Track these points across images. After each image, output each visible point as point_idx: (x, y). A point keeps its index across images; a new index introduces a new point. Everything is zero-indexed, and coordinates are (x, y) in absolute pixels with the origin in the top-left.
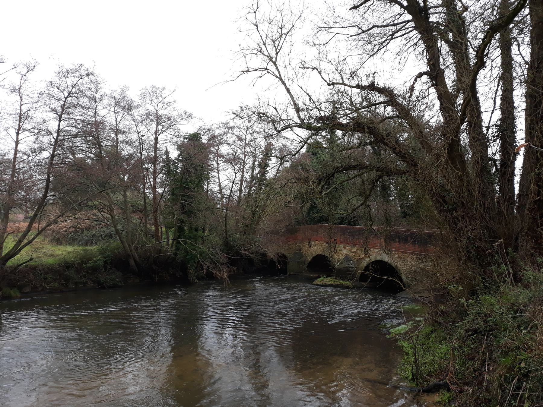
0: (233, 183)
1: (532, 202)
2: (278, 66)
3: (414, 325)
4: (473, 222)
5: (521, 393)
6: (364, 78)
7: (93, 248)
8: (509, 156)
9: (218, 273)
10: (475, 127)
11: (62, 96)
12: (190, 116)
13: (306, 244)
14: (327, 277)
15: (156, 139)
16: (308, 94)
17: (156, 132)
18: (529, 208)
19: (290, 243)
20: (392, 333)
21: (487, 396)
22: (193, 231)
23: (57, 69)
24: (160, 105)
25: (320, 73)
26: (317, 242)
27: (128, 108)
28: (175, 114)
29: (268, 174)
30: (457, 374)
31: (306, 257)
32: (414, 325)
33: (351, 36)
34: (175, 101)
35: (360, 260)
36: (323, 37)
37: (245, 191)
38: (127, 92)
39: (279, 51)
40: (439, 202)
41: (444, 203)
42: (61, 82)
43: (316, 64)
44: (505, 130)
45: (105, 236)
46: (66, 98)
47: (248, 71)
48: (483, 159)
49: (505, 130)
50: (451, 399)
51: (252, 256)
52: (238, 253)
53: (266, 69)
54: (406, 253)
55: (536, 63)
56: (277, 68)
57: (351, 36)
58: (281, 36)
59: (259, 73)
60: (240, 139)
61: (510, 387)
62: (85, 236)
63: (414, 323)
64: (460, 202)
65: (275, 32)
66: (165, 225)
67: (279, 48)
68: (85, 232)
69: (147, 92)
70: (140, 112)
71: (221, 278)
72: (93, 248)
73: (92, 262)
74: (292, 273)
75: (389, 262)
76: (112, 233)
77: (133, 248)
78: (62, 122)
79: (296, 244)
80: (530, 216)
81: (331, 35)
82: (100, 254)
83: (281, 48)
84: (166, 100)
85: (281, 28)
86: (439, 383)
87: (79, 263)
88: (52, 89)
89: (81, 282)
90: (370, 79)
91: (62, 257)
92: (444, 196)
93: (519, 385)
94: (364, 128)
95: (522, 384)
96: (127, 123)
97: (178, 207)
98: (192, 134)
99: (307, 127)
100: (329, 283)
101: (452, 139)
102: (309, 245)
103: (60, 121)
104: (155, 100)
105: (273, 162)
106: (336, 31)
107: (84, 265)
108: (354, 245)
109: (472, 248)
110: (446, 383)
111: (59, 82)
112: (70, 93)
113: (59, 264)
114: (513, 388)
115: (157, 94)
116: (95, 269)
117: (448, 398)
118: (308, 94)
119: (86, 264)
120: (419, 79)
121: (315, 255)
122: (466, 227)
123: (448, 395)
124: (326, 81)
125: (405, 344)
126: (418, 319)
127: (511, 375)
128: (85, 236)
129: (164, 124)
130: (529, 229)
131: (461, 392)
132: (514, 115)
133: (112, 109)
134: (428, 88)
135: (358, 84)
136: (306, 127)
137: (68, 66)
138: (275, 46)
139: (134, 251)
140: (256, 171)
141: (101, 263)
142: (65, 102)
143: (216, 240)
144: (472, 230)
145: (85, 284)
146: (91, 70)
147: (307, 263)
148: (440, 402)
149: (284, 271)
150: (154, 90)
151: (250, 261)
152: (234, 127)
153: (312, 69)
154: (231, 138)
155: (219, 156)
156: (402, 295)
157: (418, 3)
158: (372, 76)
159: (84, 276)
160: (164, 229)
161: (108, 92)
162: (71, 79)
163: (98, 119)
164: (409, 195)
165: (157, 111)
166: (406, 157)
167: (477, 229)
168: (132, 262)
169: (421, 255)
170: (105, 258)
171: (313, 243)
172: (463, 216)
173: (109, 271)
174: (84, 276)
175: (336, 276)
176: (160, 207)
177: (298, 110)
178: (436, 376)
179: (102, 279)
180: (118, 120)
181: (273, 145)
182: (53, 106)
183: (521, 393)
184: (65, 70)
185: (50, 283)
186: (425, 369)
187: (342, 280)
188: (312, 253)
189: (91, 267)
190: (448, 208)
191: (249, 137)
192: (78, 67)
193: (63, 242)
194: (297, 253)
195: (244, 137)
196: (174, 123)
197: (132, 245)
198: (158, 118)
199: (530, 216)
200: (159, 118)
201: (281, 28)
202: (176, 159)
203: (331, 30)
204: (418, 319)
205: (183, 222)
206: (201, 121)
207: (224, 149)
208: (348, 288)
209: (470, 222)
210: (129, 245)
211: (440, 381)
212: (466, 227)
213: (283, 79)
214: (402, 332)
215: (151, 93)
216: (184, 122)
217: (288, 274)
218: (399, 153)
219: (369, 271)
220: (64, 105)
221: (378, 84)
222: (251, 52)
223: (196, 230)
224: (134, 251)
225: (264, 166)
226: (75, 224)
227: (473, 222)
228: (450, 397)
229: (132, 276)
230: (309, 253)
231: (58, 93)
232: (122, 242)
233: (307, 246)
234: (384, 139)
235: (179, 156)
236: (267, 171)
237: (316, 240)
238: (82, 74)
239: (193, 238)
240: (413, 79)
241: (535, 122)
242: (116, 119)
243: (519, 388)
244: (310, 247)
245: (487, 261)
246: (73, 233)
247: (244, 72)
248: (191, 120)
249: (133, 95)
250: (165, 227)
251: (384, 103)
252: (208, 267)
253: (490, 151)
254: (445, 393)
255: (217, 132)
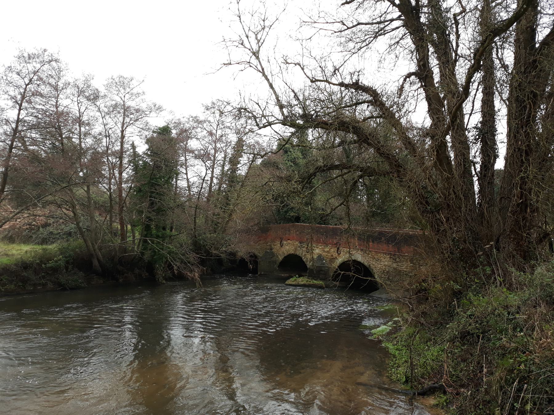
0: (204, 180)
1: (514, 204)
2: (261, 60)
3: (394, 325)
4: (458, 224)
5: (522, 395)
6: (348, 77)
7: (52, 247)
8: (490, 159)
9: (189, 274)
10: (458, 129)
11: (21, 83)
12: (160, 109)
13: (278, 243)
14: (299, 277)
15: (122, 132)
16: (293, 91)
17: (123, 124)
18: (512, 211)
19: (261, 242)
20: (375, 334)
21: (488, 398)
22: (161, 230)
23: (17, 53)
24: (127, 96)
25: (303, 69)
26: (289, 241)
27: (94, 97)
28: (143, 106)
29: (239, 171)
30: (452, 376)
31: (277, 257)
32: (394, 325)
33: (335, 32)
34: (144, 93)
35: (333, 260)
36: (307, 31)
37: (215, 187)
38: (92, 81)
39: (262, 45)
40: (421, 203)
41: (427, 204)
42: (21, 67)
43: (298, 59)
44: (486, 133)
45: (64, 234)
46: (27, 85)
47: (230, 64)
48: (465, 162)
49: (486, 133)
50: (448, 401)
51: (223, 256)
52: (208, 253)
53: (249, 63)
54: (379, 253)
55: (523, 68)
56: (260, 62)
57: (335, 32)
58: (263, 29)
59: (241, 67)
60: (211, 134)
61: (511, 390)
62: (41, 234)
63: (393, 324)
64: (446, 204)
65: (257, 23)
66: (130, 223)
67: (262, 41)
68: (41, 229)
69: (114, 82)
70: (107, 103)
71: (193, 278)
72: (52, 247)
73: (52, 262)
74: (263, 273)
75: (362, 262)
76: (72, 230)
77: (96, 247)
78: (22, 111)
79: (267, 243)
80: (512, 219)
81: (314, 31)
82: (61, 254)
83: (264, 41)
84: (135, 91)
85: (264, 21)
86: (434, 385)
87: (37, 263)
88: (10, 75)
89: (40, 284)
90: (355, 78)
91: (19, 257)
92: (427, 197)
93: (520, 387)
94: (348, 127)
95: (523, 386)
96: (92, 114)
97: (145, 204)
98: (162, 128)
99: (291, 124)
100: (302, 283)
101: (441, 141)
102: (280, 244)
103: (20, 110)
104: (122, 91)
105: (244, 159)
106: (321, 26)
107: (43, 266)
108: (326, 244)
109: (456, 249)
110: (442, 385)
111: (19, 68)
112: (31, 80)
113: (16, 265)
114: (514, 389)
115: (125, 84)
116: (55, 270)
117: (445, 401)
118: (293, 91)
119: (45, 264)
120: (408, 79)
121: (287, 254)
122: (451, 229)
123: (445, 398)
124: (308, 77)
125: (390, 346)
126: (396, 319)
127: (511, 378)
128: (41, 234)
129: (132, 116)
130: (511, 231)
131: (458, 394)
132: (494, 118)
133: (75, 99)
134: (417, 89)
135: (342, 82)
136: (289, 124)
137: (31, 50)
138: (257, 38)
139: (98, 250)
140: (226, 168)
141: (62, 263)
142: (25, 89)
143: (184, 238)
144: (457, 232)
145: (44, 285)
146: (56, 56)
147: (278, 263)
148: (437, 405)
149: (255, 271)
150: (121, 79)
151: (220, 261)
152: (205, 121)
153: (294, 65)
154: (201, 133)
155: (187, 150)
156: (376, 294)
157: (410, 2)
158: (356, 74)
159: (44, 277)
160: (129, 227)
161: (71, 81)
162: (32, 65)
163: (60, 109)
164: (81, 177)
165: (124, 102)
166: (389, 158)
167: (462, 231)
168: (95, 263)
169: (394, 255)
170: (66, 257)
171: (285, 242)
172: (448, 218)
173: (70, 271)
174: (44, 277)
175: (309, 276)
176: (126, 204)
177: (281, 107)
178: (430, 379)
179: (63, 280)
180: (82, 110)
181: (244, 141)
182: (12, 93)
183: (522, 395)
184: (26, 55)
185: (6, 285)
186: (418, 371)
187: (315, 280)
188: (283, 253)
189: (51, 267)
190: (431, 209)
191: (219, 132)
192: (40, 52)
193: (16, 239)
194: (268, 252)
195: (214, 132)
196: (143, 115)
197: (95, 244)
198: (125, 110)
199: (512, 219)
200: (126, 110)
201: (264, 21)
202: (144, 153)
203: (315, 25)
204: (396, 319)
205: (151, 220)
206: (172, 114)
207: (193, 144)
208: (321, 287)
209: (454, 224)
210: (92, 244)
211: (434, 384)
212: (451, 229)
213: (266, 74)
214: (384, 333)
215: (118, 84)
216: (153, 114)
217: (259, 273)
218: (383, 153)
219: (351, 272)
220: (24, 92)
221: (362, 83)
222: (232, 44)
223: (164, 229)
224: (98, 250)
225: (234, 162)
226: (30, 221)
227: (458, 224)
228: (447, 400)
229: (95, 277)
230: (281, 253)
231: (18, 79)
232: (85, 241)
233: (279, 245)
234: (368, 139)
235: (148, 150)
236: (238, 168)
237: (289, 240)
238: (45, 60)
239: (161, 237)
240: (402, 79)
241: (520, 126)
242: (79, 109)
243: (519, 390)
244: (282, 246)
245: (471, 262)
246: (27, 231)
247: (224, 64)
248: (161, 113)
249: (99, 84)
250: (131, 225)
251: (368, 102)
252: (178, 268)
253: (472, 152)
254: (443, 396)
255: (187, 126)
